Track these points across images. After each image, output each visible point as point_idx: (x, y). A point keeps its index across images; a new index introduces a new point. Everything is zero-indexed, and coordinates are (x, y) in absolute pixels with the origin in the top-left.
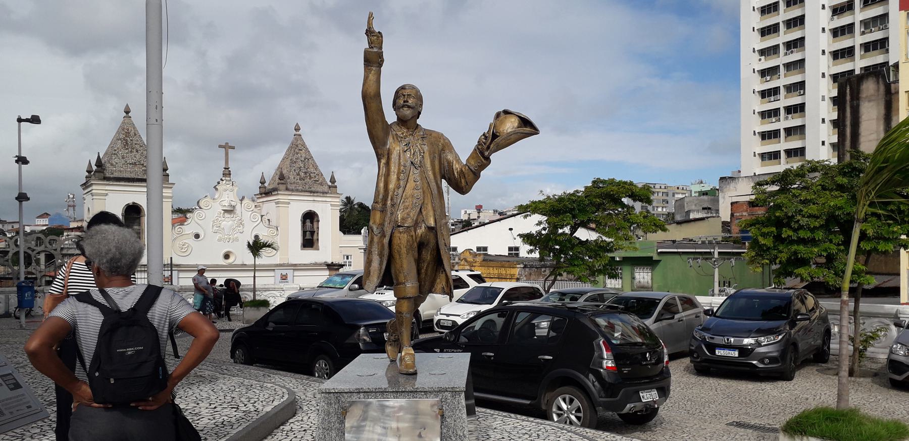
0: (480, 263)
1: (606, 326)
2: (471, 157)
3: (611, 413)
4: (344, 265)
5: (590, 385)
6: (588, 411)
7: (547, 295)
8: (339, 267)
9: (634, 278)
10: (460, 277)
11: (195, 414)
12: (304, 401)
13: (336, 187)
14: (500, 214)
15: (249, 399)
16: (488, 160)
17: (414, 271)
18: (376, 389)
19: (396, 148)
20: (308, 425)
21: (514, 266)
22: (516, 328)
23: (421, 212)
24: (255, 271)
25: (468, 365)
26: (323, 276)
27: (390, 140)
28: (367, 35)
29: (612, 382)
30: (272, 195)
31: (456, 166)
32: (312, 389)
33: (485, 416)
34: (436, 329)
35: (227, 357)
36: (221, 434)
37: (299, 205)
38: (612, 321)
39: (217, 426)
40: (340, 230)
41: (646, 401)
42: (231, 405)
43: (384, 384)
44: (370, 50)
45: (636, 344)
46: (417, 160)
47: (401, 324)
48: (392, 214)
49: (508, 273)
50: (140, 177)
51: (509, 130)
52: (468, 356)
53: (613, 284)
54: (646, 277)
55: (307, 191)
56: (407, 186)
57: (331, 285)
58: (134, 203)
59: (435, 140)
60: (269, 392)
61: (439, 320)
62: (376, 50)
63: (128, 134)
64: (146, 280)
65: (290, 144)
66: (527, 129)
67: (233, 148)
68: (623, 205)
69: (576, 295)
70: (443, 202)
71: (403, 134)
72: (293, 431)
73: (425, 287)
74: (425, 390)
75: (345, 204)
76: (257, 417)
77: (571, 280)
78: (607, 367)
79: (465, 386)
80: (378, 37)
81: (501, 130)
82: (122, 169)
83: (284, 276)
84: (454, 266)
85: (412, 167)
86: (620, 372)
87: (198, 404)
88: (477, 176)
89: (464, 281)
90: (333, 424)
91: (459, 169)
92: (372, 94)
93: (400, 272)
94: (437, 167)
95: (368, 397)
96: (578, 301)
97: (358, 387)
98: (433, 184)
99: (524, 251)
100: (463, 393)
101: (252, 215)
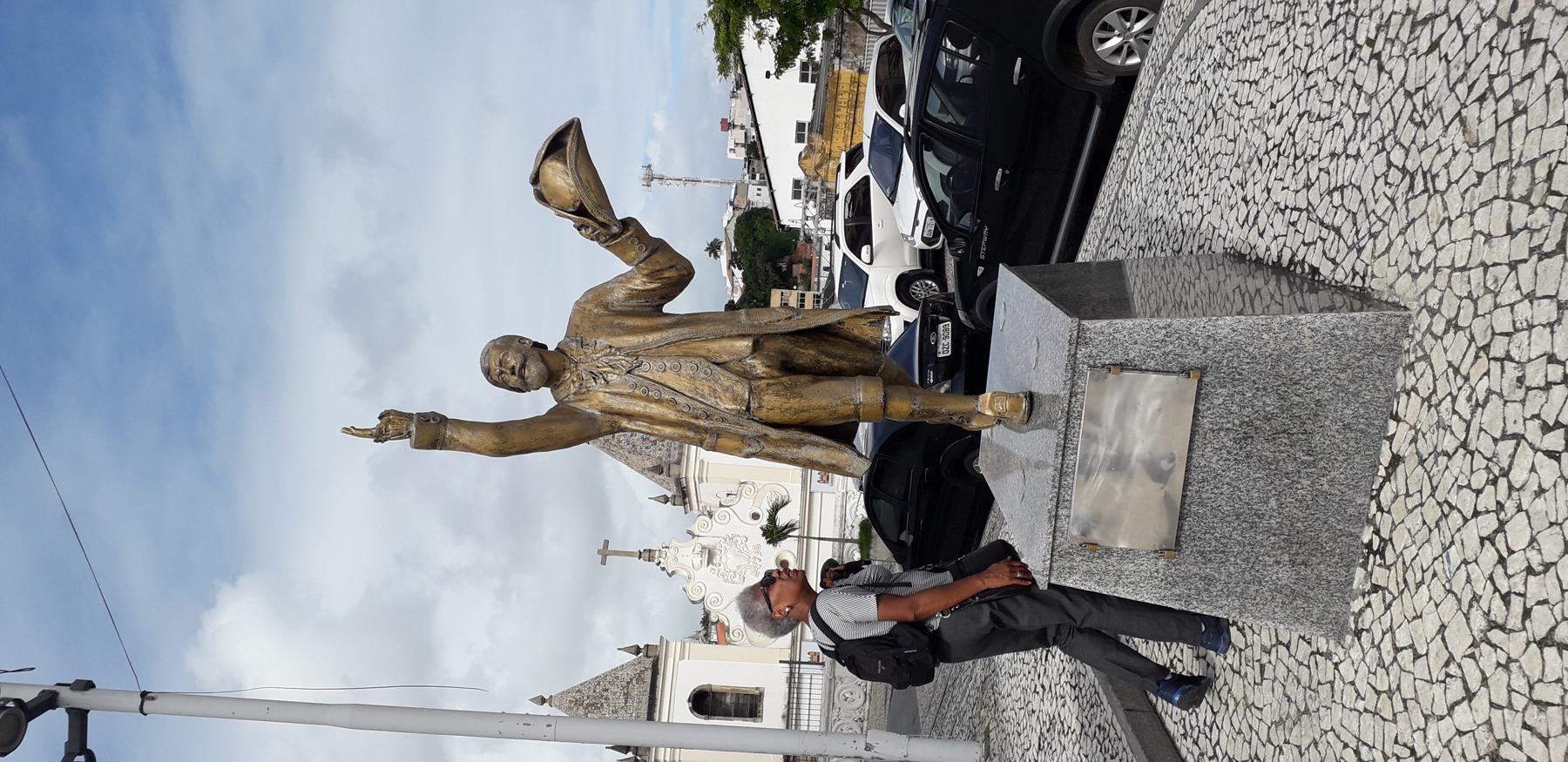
0: (826, 140)
10: (850, 190)
11: (1051, 724)
16: (627, 223)
18: (1054, 487)
19: (599, 399)
21: (836, 76)
23: (722, 363)
24: (809, 538)
27: (584, 406)
30: (687, 487)
31: (639, 283)
34: (938, 245)
36: (1093, 699)
39: (1077, 697)
42: (1041, 659)
44: (413, 437)
48: (724, 419)
50: (648, 689)
51: (571, 181)
56: (672, 386)
58: (689, 701)
59: (586, 320)
61: (924, 239)
62: (414, 429)
63: (578, 703)
64: (806, 728)
65: (602, 452)
67: (606, 542)
71: (573, 382)
73: (867, 359)
74: (1068, 395)
81: (569, 197)
82: (634, 715)
85: (636, 372)
87: (1033, 712)
88: (659, 246)
89: (854, 186)
90: (1110, 568)
91: (644, 280)
92: (497, 440)
93: (835, 412)
94: (639, 322)
95: (1068, 500)
97: (1046, 517)
98: (671, 334)
100: (1084, 322)
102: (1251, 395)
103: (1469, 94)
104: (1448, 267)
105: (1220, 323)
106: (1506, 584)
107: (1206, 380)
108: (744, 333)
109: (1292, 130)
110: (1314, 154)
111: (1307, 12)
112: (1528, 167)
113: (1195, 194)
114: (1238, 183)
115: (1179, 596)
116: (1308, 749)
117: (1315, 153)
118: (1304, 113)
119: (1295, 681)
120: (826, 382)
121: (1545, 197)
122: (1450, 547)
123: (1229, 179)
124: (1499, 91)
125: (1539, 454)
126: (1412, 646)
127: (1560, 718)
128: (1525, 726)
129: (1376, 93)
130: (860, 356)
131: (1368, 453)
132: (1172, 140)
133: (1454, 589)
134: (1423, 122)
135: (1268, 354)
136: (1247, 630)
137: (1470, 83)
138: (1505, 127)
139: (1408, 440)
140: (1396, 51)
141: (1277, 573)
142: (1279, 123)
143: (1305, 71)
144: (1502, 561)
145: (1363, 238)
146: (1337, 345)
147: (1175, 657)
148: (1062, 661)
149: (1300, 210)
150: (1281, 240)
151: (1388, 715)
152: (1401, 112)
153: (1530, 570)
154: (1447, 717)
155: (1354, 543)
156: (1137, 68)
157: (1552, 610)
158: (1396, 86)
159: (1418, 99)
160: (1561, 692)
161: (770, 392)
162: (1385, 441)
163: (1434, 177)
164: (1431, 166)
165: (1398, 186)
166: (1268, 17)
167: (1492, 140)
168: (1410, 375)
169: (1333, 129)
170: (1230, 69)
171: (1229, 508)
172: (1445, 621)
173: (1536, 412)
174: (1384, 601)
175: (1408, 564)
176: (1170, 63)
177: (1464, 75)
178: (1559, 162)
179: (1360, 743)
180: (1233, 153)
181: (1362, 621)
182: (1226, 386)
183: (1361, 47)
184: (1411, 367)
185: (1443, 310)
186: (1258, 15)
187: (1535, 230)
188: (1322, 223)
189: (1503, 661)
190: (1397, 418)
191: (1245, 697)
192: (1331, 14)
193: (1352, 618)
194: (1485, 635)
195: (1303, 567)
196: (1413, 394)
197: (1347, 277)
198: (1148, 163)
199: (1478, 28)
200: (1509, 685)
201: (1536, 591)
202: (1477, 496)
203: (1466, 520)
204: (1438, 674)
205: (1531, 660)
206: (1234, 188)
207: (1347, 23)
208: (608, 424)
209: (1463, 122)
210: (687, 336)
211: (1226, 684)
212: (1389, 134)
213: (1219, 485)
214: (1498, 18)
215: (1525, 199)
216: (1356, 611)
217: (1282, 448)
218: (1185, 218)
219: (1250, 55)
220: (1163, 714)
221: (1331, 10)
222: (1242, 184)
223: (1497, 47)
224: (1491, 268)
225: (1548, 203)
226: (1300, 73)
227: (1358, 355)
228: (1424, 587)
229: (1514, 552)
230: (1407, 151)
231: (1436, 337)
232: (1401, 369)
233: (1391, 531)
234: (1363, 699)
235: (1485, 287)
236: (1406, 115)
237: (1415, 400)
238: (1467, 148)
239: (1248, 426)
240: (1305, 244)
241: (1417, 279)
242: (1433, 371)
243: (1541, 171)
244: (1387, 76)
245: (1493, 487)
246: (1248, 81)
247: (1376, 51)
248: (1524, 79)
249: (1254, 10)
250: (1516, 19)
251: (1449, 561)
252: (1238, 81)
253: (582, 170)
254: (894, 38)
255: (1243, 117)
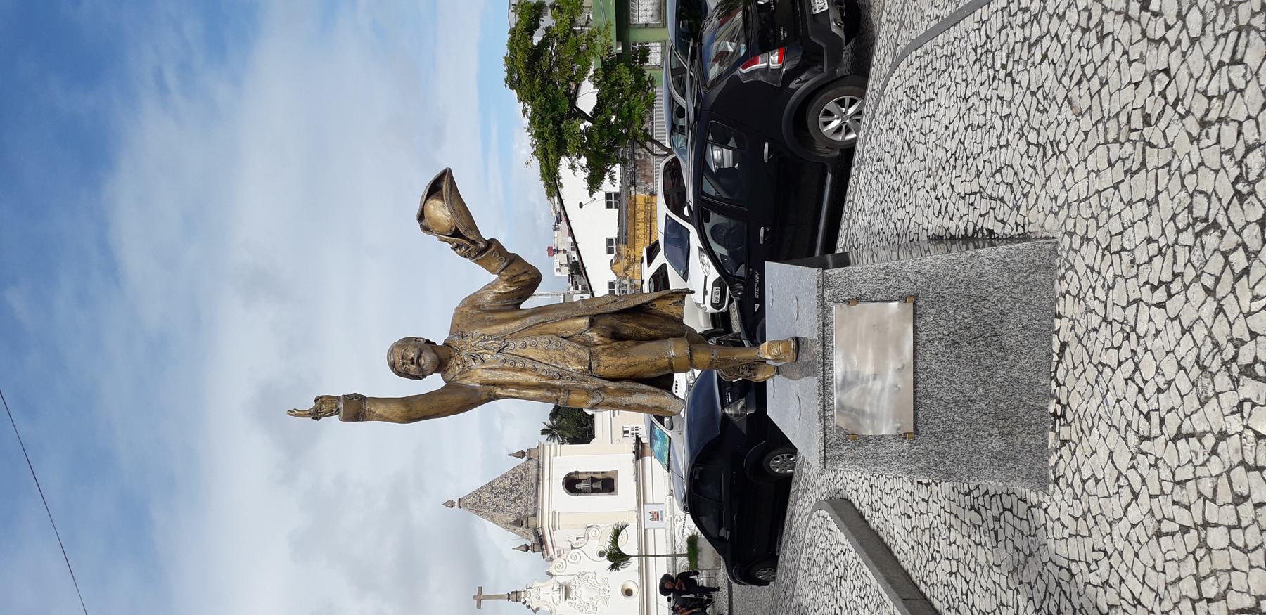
1: (720, 64)
2: (487, 267)
3: (844, 55)
4: (637, 437)
5: (804, 86)
6: (841, 88)
7: (675, 152)
8: (640, 443)
9: (647, 25)
12: (830, 488)
13: (530, 450)
14: (559, 220)
15: (828, 562)
17: (653, 345)
19: (478, 375)
20: (863, 483)
21: (633, 200)
22: (725, 196)
24: (646, 556)
25: (783, 265)
26: (653, 465)
27: (468, 382)
28: (321, 418)
29: (801, 54)
30: (543, 535)
31: (502, 288)
32: (812, 477)
33: (851, 238)
34: (724, 309)
35: (767, 591)
36: (878, 601)
37: (555, 498)
38: (713, 56)
39: (866, 605)
40: (588, 443)
41: (826, 4)
42: (837, 586)
43: (813, 382)
45: (745, 20)
46: (496, 344)
47: (727, 361)
48: (573, 378)
49: (643, 209)
51: (449, 214)
52: (769, 265)
53: (655, 56)
54: (644, 7)
55: (537, 489)
56: (532, 357)
57: (666, 454)
60: (818, 535)
61: (712, 305)
62: (342, 405)
66: (444, 187)
67: (480, 589)
68: (544, 43)
69: (675, 110)
70: (554, 307)
72: (872, 502)
73: (674, 328)
75: (553, 436)
76: (854, 551)
77: (652, 117)
78: (779, 62)
79: (816, 269)
80: (322, 402)
81: (447, 224)
83: (653, 516)
84: (635, 286)
86: (786, 42)
88: (514, 259)
89: (657, 271)
90: (869, 452)
91: (506, 285)
92: (404, 409)
93: (654, 365)
94: (504, 316)
95: (831, 404)
96: (685, 107)
97: (817, 420)
98: (529, 321)
99: (607, 186)
100: (826, 271)
101: (572, 561)
102: (952, 311)
103: (1070, 82)
104: (1075, 201)
105: (923, 261)
106: (1146, 406)
107: (919, 304)
108: (582, 314)
109: (962, 140)
110: (979, 152)
111: (961, 58)
112: (1115, 119)
113: (903, 205)
114: (931, 188)
115: (922, 468)
116: (1036, 582)
117: (979, 151)
118: (968, 127)
119: (1020, 534)
120: (646, 344)
121: (1128, 134)
122: (1106, 394)
123: (924, 188)
124: (1089, 74)
125: (1153, 307)
126: (1093, 475)
127: (1195, 487)
128: (1175, 503)
129: (1013, 99)
130: (669, 326)
131: (1043, 345)
132: (882, 173)
133: (1115, 423)
134: (1045, 109)
135: (960, 280)
136: (982, 510)
137: (1070, 74)
138: (1097, 96)
139: (1069, 329)
140: (1021, 67)
141: (991, 443)
142: (952, 138)
143: (965, 97)
144: (1141, 391)
145: (1019, 199)
146: (1009, 269)
147: (934, 550)
148: (852, 581)
149: (975, 193)
150: (965, 218)
151: (1085, 533)
152: (1030, 106)
153: (1159, 391)
154: (1124, 518)
155: (1044, 414)
156: (854, 141)
157: (1177, 413)
158: (1025, 91)
159: (1040, 95)
160: (1192, 469)
161: (605, 354)
162: (1054, 335)
163: (1057, 144)
164: (1054, 137)
165: (1036, 156)
166: (935, 69)
167: (1090, 108)
168: (1064, 283)
169: (989, 132)
170: (915, 112)
171: (949, 398)
172: (1112, 448)
173: (1146, 280)
174: (1070, 450)
175: (1082, 417)
176: (874, 120)
177: (1066, 70)
178: (1133, 109)
179: (1070, 562)
180: (925, 169)
181: (1058, 471)
182: (933, 307)
183: (998, 71)
184: (1063, 277)
185: (1078, 231)
186: (929, 70)
187: (1125, 159)
188: (991, 198)
189: (1153, 463)
190: (1059, 317)
191: (987, 561)
192: (976, 55)
193: (1051, 471)
194: (1139, 448)
195: (1009, 436)
196: (1067, 295)
197: (1012, 229)
198: (867, 195)
199: (1070, 38)
200: (1159, 478)
201: (1165, 403)
202: (1119, 351)
203: (1114, 371)
204: (1113, 489)
205: (1170, 456)
206: (928, 192)
207: (987, 58)
208: (486, 393)
209: (1070, 102)
210: (541, 321)
211: (973, 556)
212: (1025, 124)
213: (940, 381)
214: (1082, 27)
215: (1116, 141)
216: (1053, 464)
217: (980, 348)
218: (898, 225)
219: (927, 98)
220: (931, 599)
221: (976, 53)
222: (933, 188)
223: (1083, 46)
224: (1103, 193)
225: (1130, 138)
226: (961, 100)
227: (1025, 274)
228: (1095, 429)
229: (1147, 382)
230: (1038, 131)
231: (1076, 251)
232: (1057, 281)
233: (1068, 398)
234: (1067, 528)
235: (1101, 206)
236: (1034, 108)
237: (1069, 298)
238: (1075, 118)
239: (954, 335)
240: (981, 215)
241: (1057, 215)
242: (1078, 275)
243: (1123, 119)
244: (1018, 85)
245: (1127, 341)
246: (928, 116)
247: (1008, 71)
248: (1103, 62)
249: (926, 67)
250: (1092, 25)
251: (1108, 404)
252: (922, 118)
253: (455, 203)
254: (676, 158)
255: (928, 141)
